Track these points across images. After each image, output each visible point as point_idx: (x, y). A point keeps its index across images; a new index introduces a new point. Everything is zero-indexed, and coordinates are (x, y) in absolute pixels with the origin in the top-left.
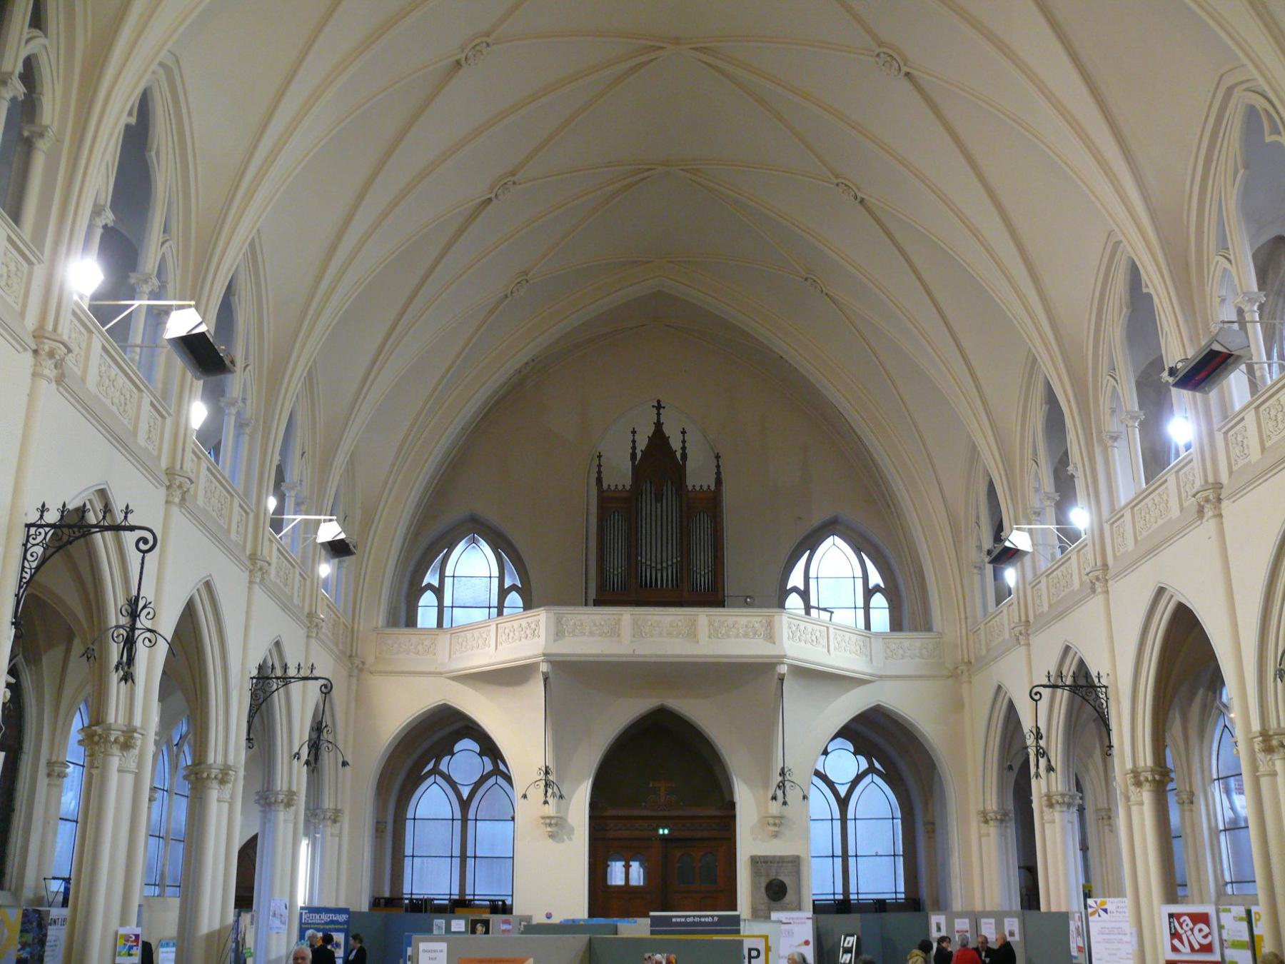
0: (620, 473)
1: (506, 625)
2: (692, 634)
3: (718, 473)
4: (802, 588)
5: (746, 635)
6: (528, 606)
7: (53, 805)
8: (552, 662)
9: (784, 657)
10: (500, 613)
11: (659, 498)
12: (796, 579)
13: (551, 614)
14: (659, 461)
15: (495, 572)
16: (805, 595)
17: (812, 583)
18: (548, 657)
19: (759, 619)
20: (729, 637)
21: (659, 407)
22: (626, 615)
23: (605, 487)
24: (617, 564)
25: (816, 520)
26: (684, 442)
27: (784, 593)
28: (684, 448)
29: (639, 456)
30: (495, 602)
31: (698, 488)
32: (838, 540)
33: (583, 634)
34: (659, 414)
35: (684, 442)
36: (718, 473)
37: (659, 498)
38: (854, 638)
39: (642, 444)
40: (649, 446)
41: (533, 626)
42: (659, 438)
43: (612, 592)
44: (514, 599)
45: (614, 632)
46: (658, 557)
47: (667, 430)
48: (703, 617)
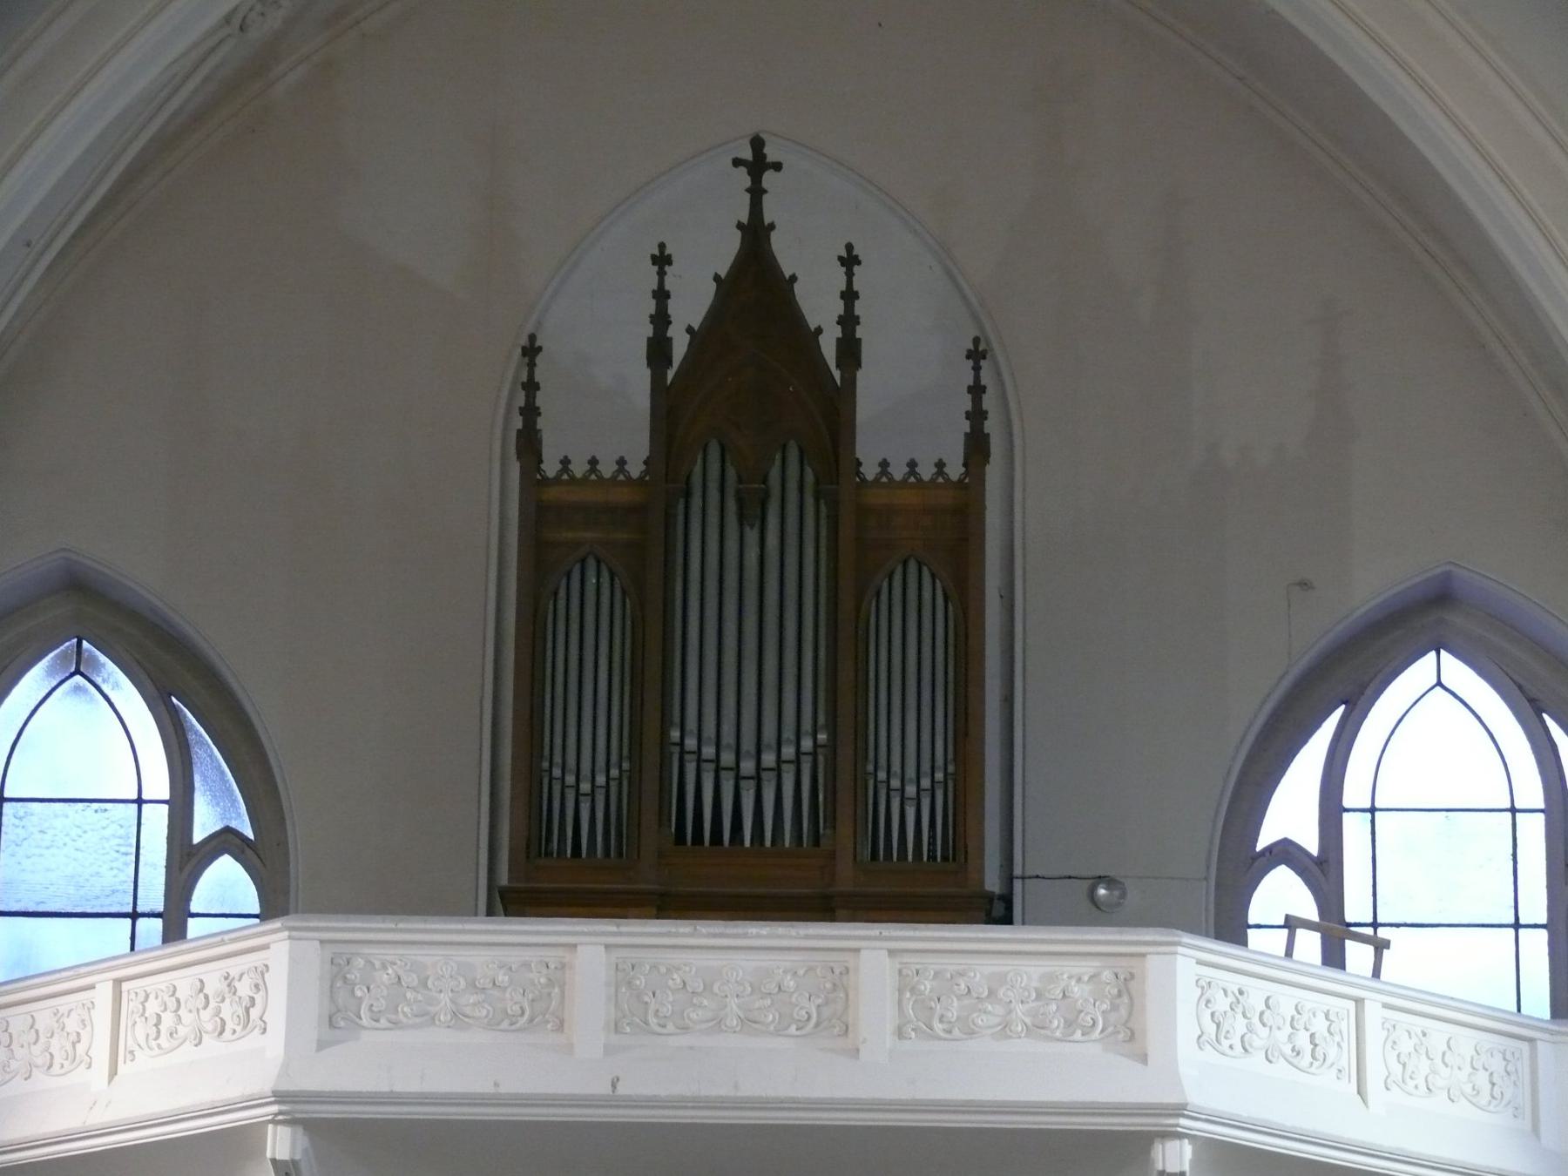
0: (606, 420)
1: (179, 979)
2: (834, 1023)
3: (977, 416)
4: (1312, 845)
5: (1038, 1028)
6: (274, 904)
7: (1194, 1152)
8: (311, 1127)
9: (1179, 1110)
10: (174, 929)
11: (752, 508)
12: (1290, 813)
13: (311, 949)
14: (755, 369)
15: (158, 783)
16: (1323, 872)
17: (1354, 829)
18: (294, 1107)
19: (1086, 967)
20: (971, 1033)
21: (758, 165)
22: (590, 950)
23: (550, 468)
24: (590, 754)
25: (1371, 584)
26: (849, 296)
27: (1242, 865)
28: (848, 321)
29: (680, 346)
30: (153, 895)
31: (898, 472)
32: (1456, 670)
33: (428, 1019)
34: (756, 193)
35: (849, 296)
36: (977, 416)
37: (752, 508)
38: (1466, 1040)
39: (691, 306)
40: (716, 315)
41: (244, 989)
42: (755, 282)
43: (548, 872)
44: (226, 883)
45: (545, 1012)
46: (745, 727)
47: (787, 253)
48: (880, 960)
